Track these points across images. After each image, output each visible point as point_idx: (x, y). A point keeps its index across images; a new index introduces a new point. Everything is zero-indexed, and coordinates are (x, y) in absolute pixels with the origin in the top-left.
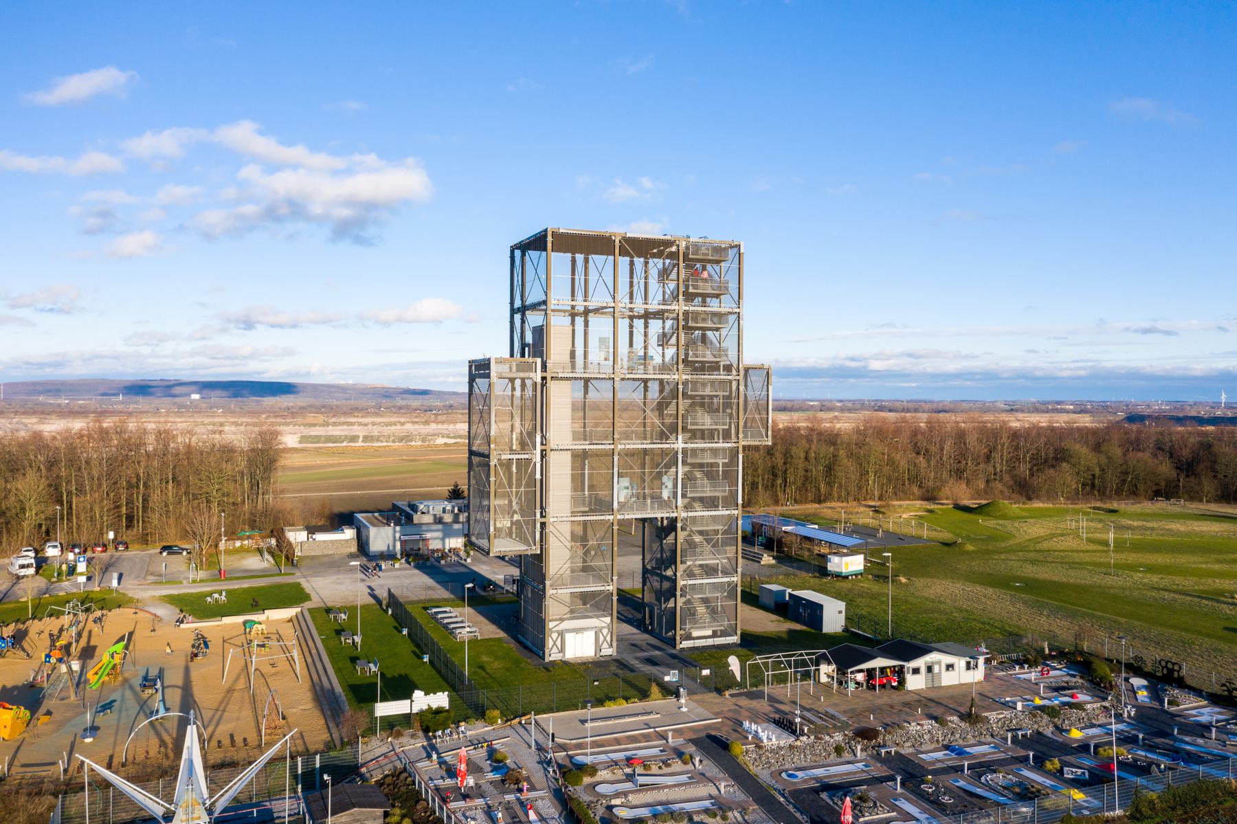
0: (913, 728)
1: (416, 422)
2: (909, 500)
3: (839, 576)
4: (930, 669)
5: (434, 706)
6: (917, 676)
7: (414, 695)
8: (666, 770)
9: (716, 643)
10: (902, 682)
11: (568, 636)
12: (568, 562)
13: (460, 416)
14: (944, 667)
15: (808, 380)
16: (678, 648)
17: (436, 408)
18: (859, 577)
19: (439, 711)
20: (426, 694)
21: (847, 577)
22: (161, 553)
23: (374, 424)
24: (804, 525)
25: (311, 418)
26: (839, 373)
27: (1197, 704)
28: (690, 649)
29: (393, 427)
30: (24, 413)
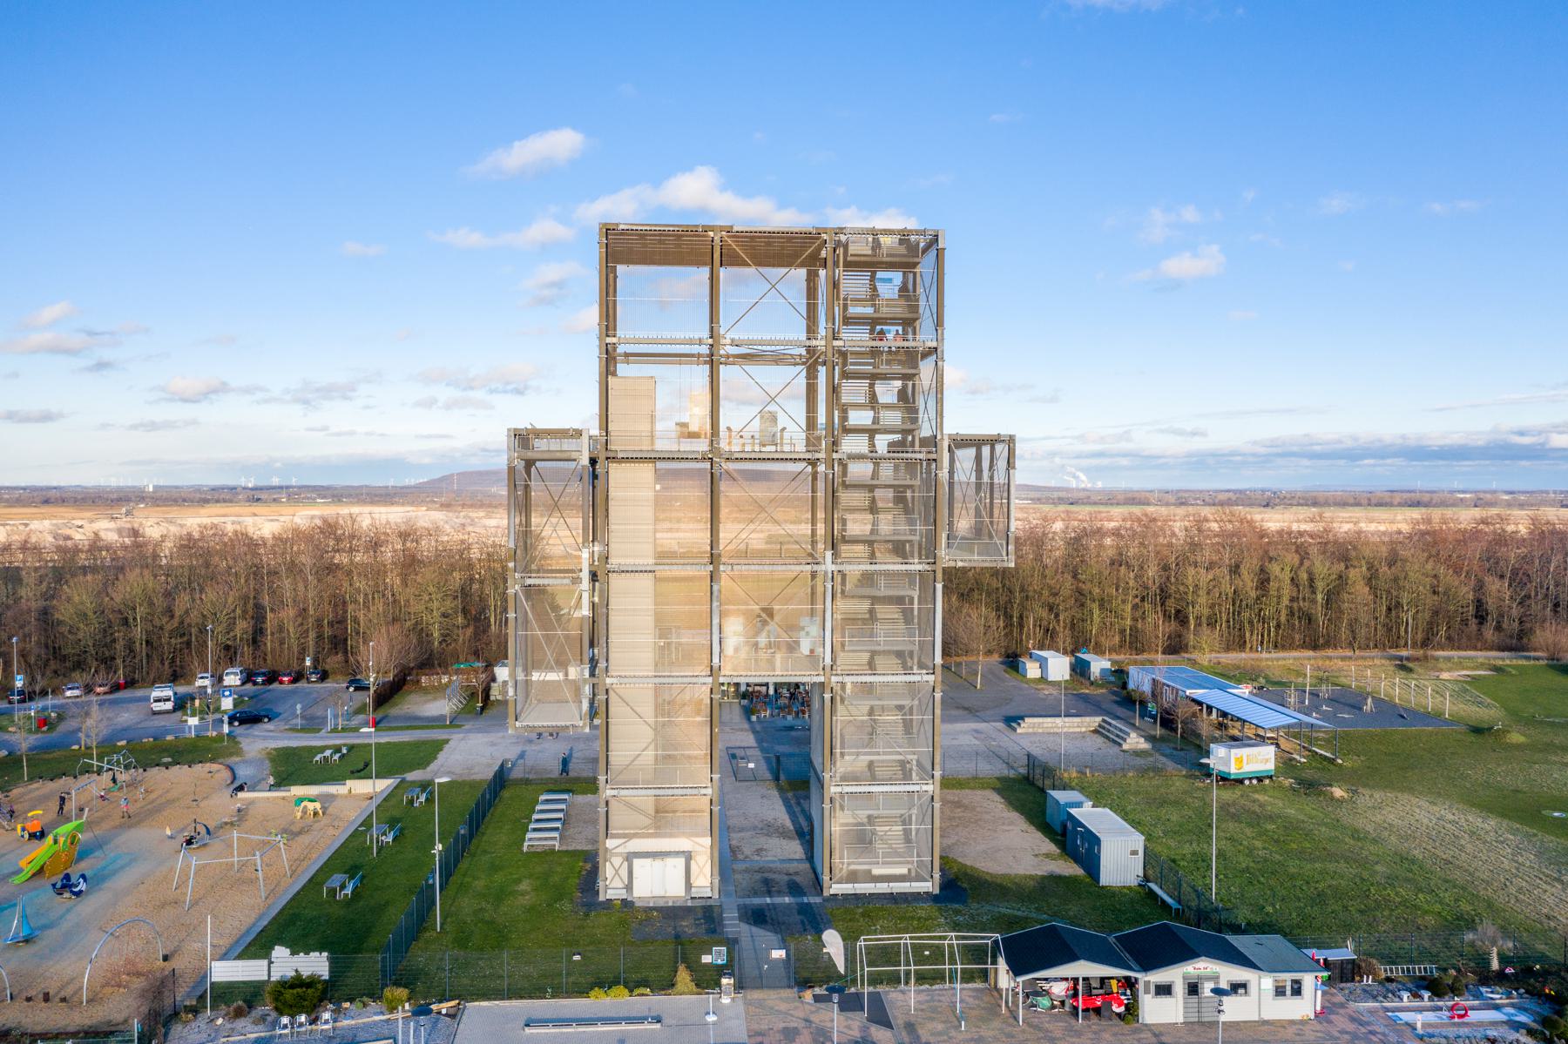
4: (1193, 989)
5: (305, 973)
6: (1164, 1000)
7: (274, 954)
9: (894, 891)
10: (1132, 1010)
11: (637, 862)
12: (652, 747)
15: (1455, 463)
16: (826, 894)
18: (1267, 782)
20: (293, 954)
21: (1241, 781)
22: (348, 688)
24: (1223, 688)
25: (779, 514)
26: (1502, 452)
28: (846, 897)
30: (472, 506)
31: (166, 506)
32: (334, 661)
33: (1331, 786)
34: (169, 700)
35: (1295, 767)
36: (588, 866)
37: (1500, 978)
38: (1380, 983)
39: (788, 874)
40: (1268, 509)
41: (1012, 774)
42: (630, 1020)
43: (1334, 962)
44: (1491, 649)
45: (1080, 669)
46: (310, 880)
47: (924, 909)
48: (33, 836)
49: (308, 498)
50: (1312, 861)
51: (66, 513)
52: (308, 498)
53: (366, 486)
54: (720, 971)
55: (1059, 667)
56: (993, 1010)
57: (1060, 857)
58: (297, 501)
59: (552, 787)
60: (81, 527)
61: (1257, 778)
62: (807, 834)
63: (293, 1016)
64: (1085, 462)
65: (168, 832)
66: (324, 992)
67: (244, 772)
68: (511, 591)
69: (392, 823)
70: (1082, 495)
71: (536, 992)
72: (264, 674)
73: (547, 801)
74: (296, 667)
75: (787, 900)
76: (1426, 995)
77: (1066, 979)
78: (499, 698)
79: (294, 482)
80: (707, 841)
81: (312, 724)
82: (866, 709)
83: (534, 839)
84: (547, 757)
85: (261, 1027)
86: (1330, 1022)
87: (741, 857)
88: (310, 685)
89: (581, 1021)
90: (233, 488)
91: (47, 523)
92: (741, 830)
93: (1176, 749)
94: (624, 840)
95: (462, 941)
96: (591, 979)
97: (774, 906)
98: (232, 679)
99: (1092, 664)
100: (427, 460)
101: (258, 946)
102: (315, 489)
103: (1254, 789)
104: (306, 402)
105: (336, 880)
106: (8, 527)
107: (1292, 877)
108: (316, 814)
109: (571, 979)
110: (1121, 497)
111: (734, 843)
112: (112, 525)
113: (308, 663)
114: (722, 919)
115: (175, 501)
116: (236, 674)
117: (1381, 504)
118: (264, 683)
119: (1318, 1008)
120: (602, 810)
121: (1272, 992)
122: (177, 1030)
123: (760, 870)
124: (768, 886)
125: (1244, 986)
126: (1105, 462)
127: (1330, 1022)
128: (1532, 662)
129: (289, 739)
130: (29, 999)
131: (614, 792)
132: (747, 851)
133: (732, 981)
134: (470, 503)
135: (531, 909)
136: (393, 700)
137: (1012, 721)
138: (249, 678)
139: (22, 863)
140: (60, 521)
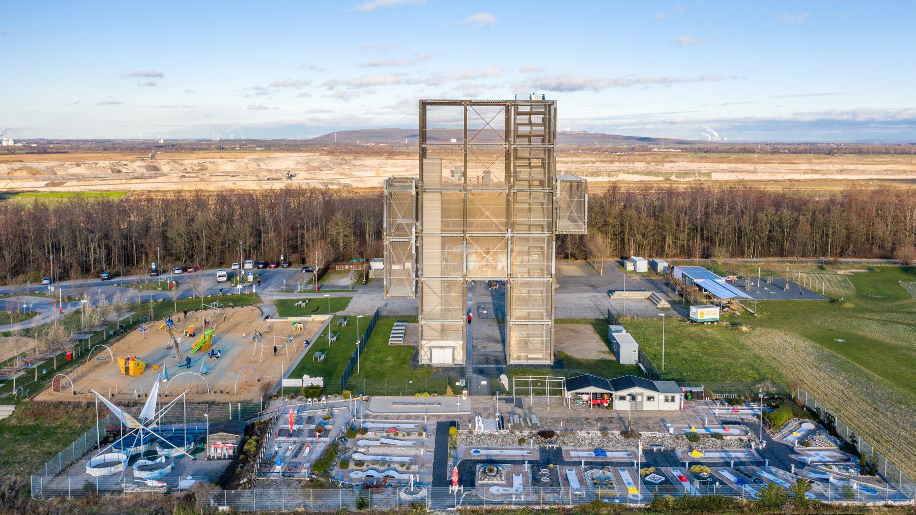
0: (582, 434)
1: (604, 161)
2: (867, 257)
3: (693, 322)
5: (315, 384)
6: (623, 402)
7: (304, 377)
8: (407, 437)
10: (611, 406)
11: (434, 350)
12: (440, 305)
13: (638, 157)
14: (645, 399)
16: (508, 364)
17: (622, 150)
18: (716, 323)
19: (317, 387)
20: (310, 377)
21: (703, 323)
23: (572, 162)
27: (825, 448)
29: (587, 165)
30: (345, 153)
31: (171, 152)
32: (294, 257)
33: (742, 326)
34: (224, 276)
36: (415, 352)
38: (713, 400)
39: (494, 357)
40: (830, 156)
41: (601, 317)
42: (429, 403)
43: (695, 392)
44: (876, 257)
45: (653, 266)
46: (306, 354)
48: (191, 335)
49: (252, 148)
51: (117, 156)
52: (252, 148)
53: (284, 140)
54: (463, 388)
55: (642, 265)
56: (561, 405)
57: (609, 353)
58: (245, 149)
59: (398, 319)
60: (126, 165)
61: (711, 322)
62: (503, 341)
63: (312, 399)
65: (244, 335)
66: (322, 392)
67: (266, 311)
68: (385, 244)
69: (334, 333)
70: (713, 146)
71: (396, 394)
72: (262, 263)
73: (397, 326)
74: (276, 260)
76: (727, 404)
77: (588, 394)
78: (373, 277)
79: (243, 137)
80: (461, 342)
81: (290, 289)
82: (527, 291)
83: (393, 341)
84: (396, 307)
85: (301, 402)
87: (476, 350)
88: (284, 269)
89: (412, 403)
91: (107, 162)
92: (478, 339)
93: (682, 308)
94: (428, 341)
95: (368, 376)
96: (416, 391)
97: (488, 368)
98: (248, 265)
99: (659, 264)
101: (297, 374)
103: (708, 326)
105: (317, 354)
106: (86, 165)
107: (702, 363)
108: (301, 329)
109: (408, 391)
110: (737, 147)
111: (474, 344)
112: (143, 164)
113: (282, 258)
116: (250, 263)
117: (902, 153)
118: (263, 268)
119: (682, 407)
120: (420, 329)
121: (663, 401)
122: (272, 402)
123: (484, 355)
124: (487, 361)
125: (653, 398)
128: (892, 265)
129: (283, 295)
130: (215, 392)
131: (425, 323)
132: (479, 347)
133: (467, 392)
134: (344, 151)
135: (393, 367)
136: (323, 278)
137: (611, 292)
138: (256, 264)
139: (193, 346)
140: (115, 162)
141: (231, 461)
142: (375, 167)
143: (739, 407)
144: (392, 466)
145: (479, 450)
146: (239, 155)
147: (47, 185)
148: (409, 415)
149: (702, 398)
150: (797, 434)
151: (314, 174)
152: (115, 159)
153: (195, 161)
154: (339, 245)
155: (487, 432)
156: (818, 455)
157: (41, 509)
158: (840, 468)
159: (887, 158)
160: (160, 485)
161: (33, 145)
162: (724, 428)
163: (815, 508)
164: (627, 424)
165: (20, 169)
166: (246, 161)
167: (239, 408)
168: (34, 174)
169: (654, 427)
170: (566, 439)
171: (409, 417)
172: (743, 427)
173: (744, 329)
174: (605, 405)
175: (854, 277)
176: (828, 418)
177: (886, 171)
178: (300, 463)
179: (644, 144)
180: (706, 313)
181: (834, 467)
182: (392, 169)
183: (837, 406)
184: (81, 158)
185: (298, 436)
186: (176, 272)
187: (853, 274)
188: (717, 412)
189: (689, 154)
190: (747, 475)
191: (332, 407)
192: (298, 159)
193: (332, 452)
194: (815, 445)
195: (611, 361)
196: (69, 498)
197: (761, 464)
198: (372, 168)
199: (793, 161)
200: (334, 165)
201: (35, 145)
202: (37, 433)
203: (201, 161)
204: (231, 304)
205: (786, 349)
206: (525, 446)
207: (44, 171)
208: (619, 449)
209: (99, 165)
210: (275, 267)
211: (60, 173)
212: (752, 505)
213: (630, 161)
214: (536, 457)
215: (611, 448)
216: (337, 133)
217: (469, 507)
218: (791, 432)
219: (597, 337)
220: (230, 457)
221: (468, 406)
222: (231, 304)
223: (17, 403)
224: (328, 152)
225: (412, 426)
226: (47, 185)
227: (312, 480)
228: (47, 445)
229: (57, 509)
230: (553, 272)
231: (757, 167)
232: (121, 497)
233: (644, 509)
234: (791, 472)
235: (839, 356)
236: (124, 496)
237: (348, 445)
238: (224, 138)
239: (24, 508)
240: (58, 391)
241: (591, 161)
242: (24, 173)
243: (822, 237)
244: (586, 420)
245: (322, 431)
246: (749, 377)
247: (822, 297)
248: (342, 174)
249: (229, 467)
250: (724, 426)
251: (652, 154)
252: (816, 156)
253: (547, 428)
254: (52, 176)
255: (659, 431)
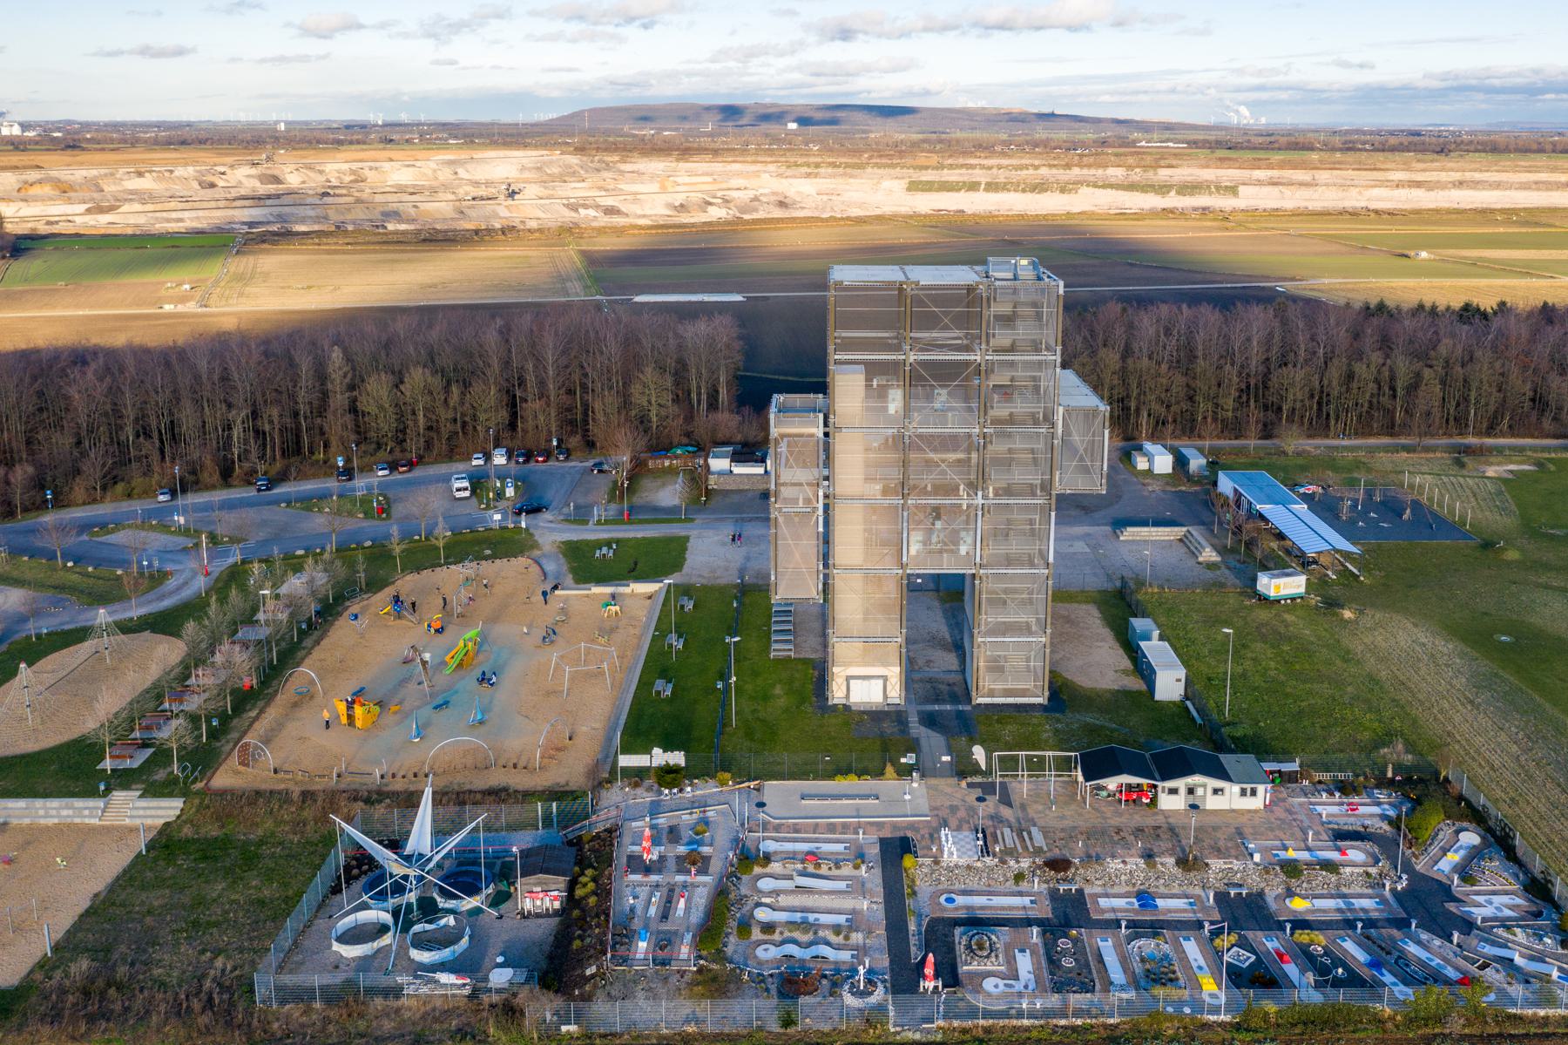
0: (1114, 865)
2: (1532, 436)
3: (1263, 599)
4: (1191, 791)
8: (835, 872)
10: (1154, 801)
11: (852, 682)
14: (1209, 791)
17: (1084, 145)
25: (922, 158)
29: (1025, 172)
30: (606, 150)
32: (574, 441)
35: (1326, 582)
37: (1391, 784)
38: (1314, 784)
40: (1442, 157)
45: (1181, 462)
47: (1037, 718)
48: (437, 631)
50: (1305, 682)
51: (206, 157)
58: (429, 142)
60: (223, 173)
62: (960, 648)
64: (1241, 96)
71: (803, 776)
75: (948, 707)
76: (1337, 794)
79: (422, 118)
80: (897, 669)
86: (1272, 812)
90: (363, 127)
91: (191, 169)
97: (940, 712)
98: (499, 459)
100: (555, 94)
102: (444, 126)
104: (435, 36)
107: (1287, 695)
112: (253, 171)
113: (555, 443)
114: (908, 722)
115: (310, 142)
118: (524, 462)
123: (930, 681)
125: (1222, 790)
126: (1264, 95)
127: (1272, 812)
141: (557, 919)
142: (658, 176)
143: (1356, 799)
144: (821, 933)
145: (953, 896)
146: (421, 154)
147: (89, 211)
148: (831, 824)
149: (1297, 781)
150: (1454, 858)
151: (554, 188)
152: (205, 163)
153: (345, 167)
154: (650, 421)
155: (962, 862)
156: (1491, 903)
157: (276, 1026)
158: (1528, 935)
159: (1541, 160)
160: (461, 982)
161: (55, 135)
162: (1338, 849)
163: (1497, 1023)
164: (1187, 850)
165: (40, 182)
166: (433, 165)
167: (555, 810)
168: (65, 190)
169: (1227, 849)
170: (1090, 875)
171: (832, 828)
172: (1368, 845)
173: (1347, 614)
174: (1145, 801)
175: (1512, 483)
176: (1503, 829)
177: (1536, 183)
178: (676, 933)
179: (1122, 131)
180: (1284, 586)
181: (1518, 931)
182: (687, 180)
183: (1512, 794)
184: (143, 161)
185: (660, 871)
186: (380, 473)
187: (1511, 477)
188: (1325, 811)
189: (1202, 153)
190: (1382, 949)
191: (702, 804)
192: (525, 161)
193: (721, 902)
194: (1484, 883)
195: (1139, 693)
196: (318, 1005)
197: (1402, 924)
198: (653, 177)
199: (1379, 165)
200: (587, 171)
201: (59, 134)
202: (229, 855)
203: (355, 166)
204: (488, 552)
205: (1419, 660)
206: (1024, 886)
207: (80, 185)
208: (1174, 891)
209: (176, 173)
210: (544, 461)
211: (110, 188)
212: (1399, 1018)
213: (1099, 166)
214: (1045, 910)
215: (1162, 890)
216: (590, 111)
217: (956, 1023)
218: (1445, 851)
219: (1107, 633)
220: (556, 913)
221: (924, 805)
222: (488, 552)
223: (185, 793)
224: (576, 149)
225: (839, 847)
226: (89, 211)
227: (700, 971)
228: (254, 883)
229: (303, 1026)
230: (1051, 560)
231: (1317, 177)
232: (400, 1003)
233: (1230, 1024)
234: (1451, 942)
235: (1507, 676)
236: (404, 1001)
237: (744, 891)
238: (391, 118)
239: (249, 1025)
240: (247, 765)
241: (1032, 165)
242: (47, 190)
243: (1458, 405)
244: (1117, 833)
245: (694, 861)
246: (1366, 729)
247: (1466, 536)
248: (600, 188)
249: (558, 933)
250: (1339, 843)
251: (1138, 153)
252: (1420, 156)
253: (1057, 851)
254: (96, 195)
255: (1237, 859)
